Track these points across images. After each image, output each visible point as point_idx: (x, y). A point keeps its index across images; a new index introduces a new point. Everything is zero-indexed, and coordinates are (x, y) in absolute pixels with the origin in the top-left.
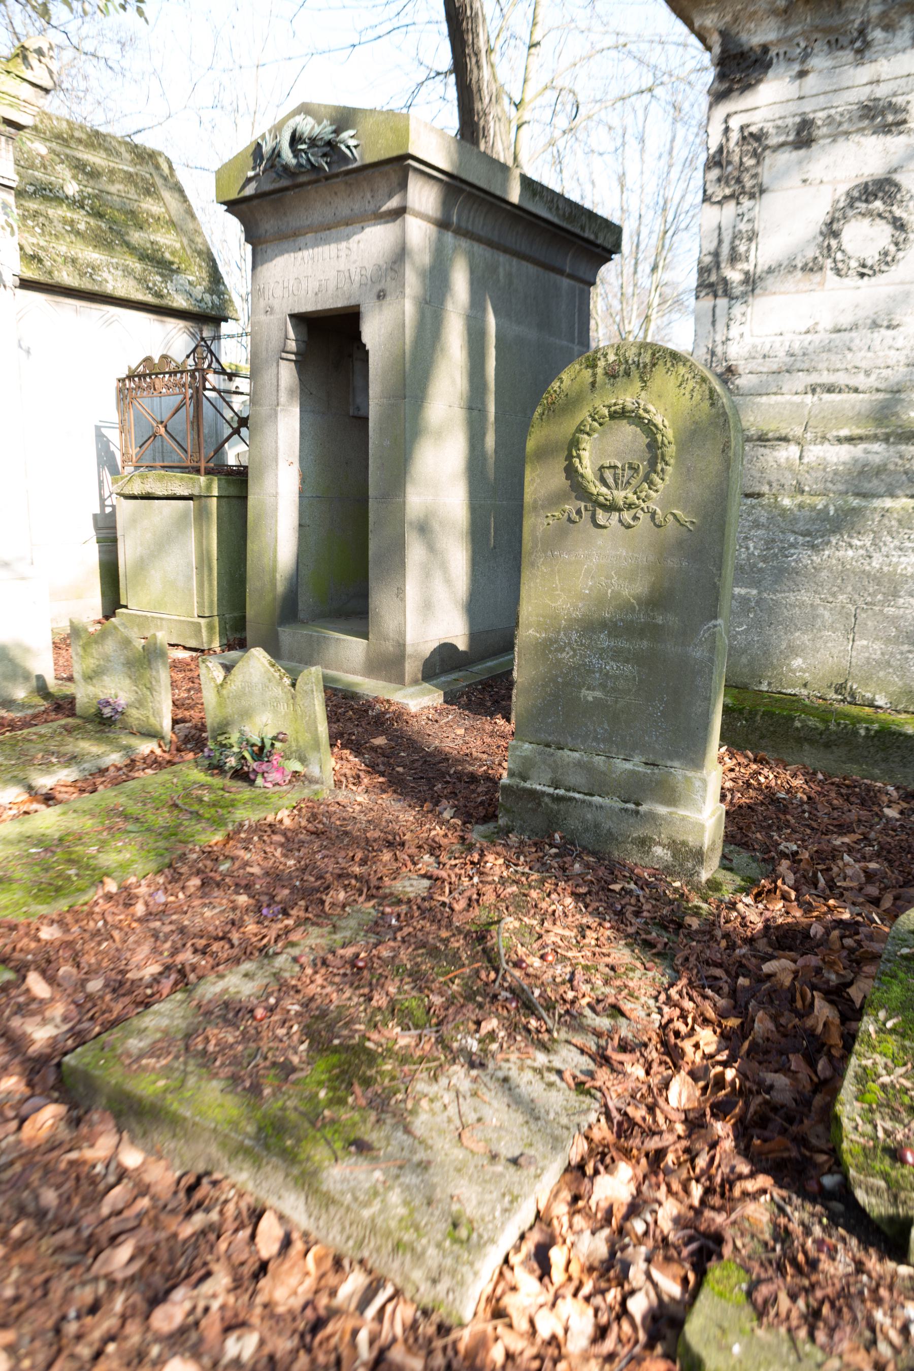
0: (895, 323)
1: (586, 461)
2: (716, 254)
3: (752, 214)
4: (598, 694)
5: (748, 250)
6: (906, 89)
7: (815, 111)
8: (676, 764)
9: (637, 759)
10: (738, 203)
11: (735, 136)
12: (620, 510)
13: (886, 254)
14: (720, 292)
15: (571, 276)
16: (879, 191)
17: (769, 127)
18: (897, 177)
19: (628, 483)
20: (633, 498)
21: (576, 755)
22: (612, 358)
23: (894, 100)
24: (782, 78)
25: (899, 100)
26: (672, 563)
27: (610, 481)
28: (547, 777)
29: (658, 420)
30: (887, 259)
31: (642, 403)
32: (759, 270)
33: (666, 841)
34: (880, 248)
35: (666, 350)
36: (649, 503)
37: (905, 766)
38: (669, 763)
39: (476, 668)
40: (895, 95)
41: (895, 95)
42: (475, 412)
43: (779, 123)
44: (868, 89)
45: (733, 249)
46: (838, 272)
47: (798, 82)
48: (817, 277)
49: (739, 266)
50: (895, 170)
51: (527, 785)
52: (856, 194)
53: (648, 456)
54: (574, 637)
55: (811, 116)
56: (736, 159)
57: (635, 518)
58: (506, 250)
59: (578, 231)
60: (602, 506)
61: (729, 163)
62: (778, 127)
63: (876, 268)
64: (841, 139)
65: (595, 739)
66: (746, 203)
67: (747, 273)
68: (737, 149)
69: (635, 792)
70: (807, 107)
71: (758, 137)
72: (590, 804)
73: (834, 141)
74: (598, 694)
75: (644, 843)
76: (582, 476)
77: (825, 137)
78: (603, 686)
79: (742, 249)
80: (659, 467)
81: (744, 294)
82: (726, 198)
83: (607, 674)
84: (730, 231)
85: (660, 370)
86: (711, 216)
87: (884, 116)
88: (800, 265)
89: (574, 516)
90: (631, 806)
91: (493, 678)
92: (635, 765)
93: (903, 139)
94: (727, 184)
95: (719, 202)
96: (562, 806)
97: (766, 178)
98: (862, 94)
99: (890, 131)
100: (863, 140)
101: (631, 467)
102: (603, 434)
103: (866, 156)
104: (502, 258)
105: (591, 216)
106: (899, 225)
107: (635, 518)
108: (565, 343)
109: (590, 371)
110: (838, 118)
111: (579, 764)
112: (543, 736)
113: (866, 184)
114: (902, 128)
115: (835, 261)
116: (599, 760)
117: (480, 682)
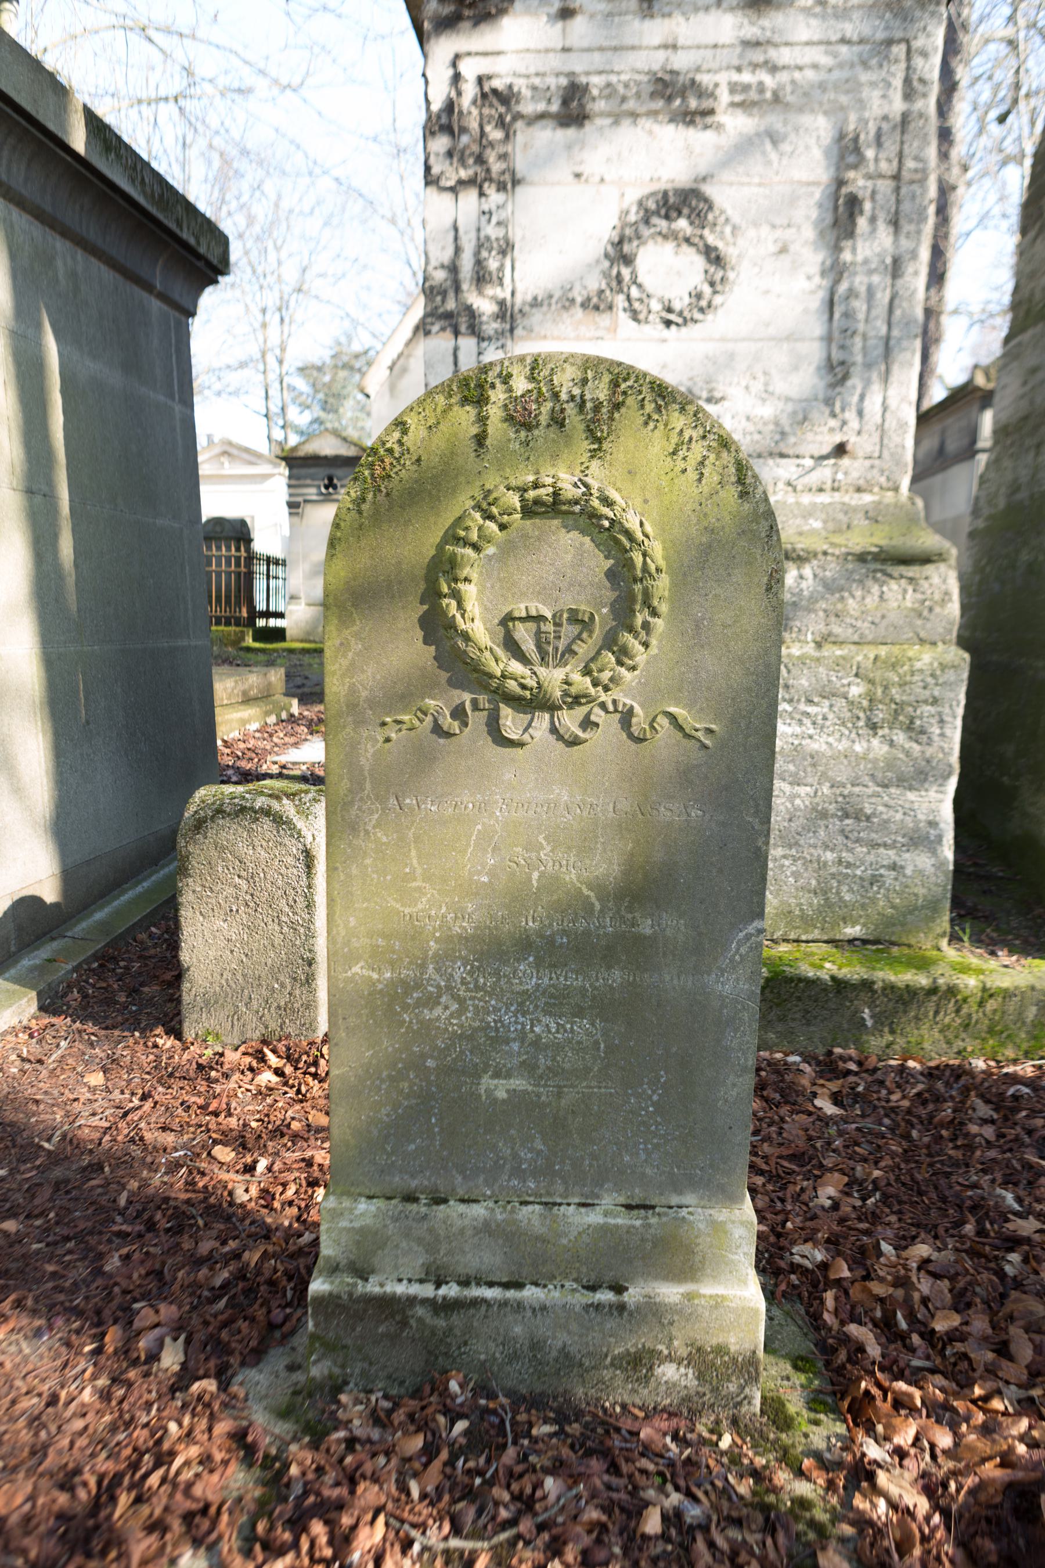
0: (717, 395)
1: (472, 606)
2: (453, 269)
3: (503, 215)
4: (518, 1083)
5: (501, 268)
6: (714, 65)
7: (588, 74)
8: (689, 1199)
9: (608, 1200)
10: (482, 194)
11: (470, 90)
12: (552, 708)
13: (699, 296)
14: (463, 328)
15: (163, 297)
16: (681, 206)
17: (521, 85)
18: (708, 190)
19: (570, 651)
20: (582, 683)
21: (478, 1211)
22: (521, 385)
23: (698, 78)
24: (536, 14)
25: (705, 79)
26: (670, 813)
27: (529, 646)
28: (416, 1262)
29: (632, 522)
30: (701, 305)
31: (595, 484)
32: (519, 300)
33: (683, 1352)
34: (691, 288)
35: (641, 376)
36: (616, 693)
37: (808, 1024)
38: (675, 1200)
39: (81, 927)
40: (698, 69)
41: (698, 69)
42: (38, 499)
43: (537, 81)
44: (661, 55)
45: (479, 263)
46: (635, 316)
47: (560, 25)
48: (604, 320)
49: (490, 291)
50: (704, 179)
51: (372, 1287)
52: (652, 205)
53: (610, 595)
54: (459, 972)
55: (583, 80)
56: (474, 125)
57: (587, 723)
58: (65, 233)
59: (173, 226)
60: (513, 700)
61: (463, 130)
62: (534, 88)
63: (686, 314)
64: (626, 122)
65: (517, 1172)
66: (495, 197)
67: (502, 303)
68: (475, 112)
69: (606, 1269)
70: (578, 64)
71: (505, 98)
72: (519, 1306)
73: (616, 123)
74: (518, 1083)
75: (639, 1364)
76: (466, 637)
77: (602, 114)
78: (529, 1068)
79: (493, 264)
80: (639, 619)
81: (500, 334)
82: (461, 182)
83: (536, 1043)
84: (473, 235)
85: (630, 416)
86: (442, 208)
87: (684, 98)
88: (579, 300)
89: (448, 722)
90: (605, 1296)
91: (113, 944)
92: (604, 1214)
93: (709, 135)
94: (462, 162)
95: (452, 189)
96: (457, 1320)
97: (520, 165)
98: (656, 61)
99: (692, 122)
100: (656, 128)
101: (574, 617)
102: (508, 550)
103: (656, 154)
104: (60, 245)
105: (190, 209)
106: (714, 257)
107: (587, 723)
108: (162, 398)
109: (471, 411)
110: (621, 90)
111: (486, 1229)
112: (398, 1181)
113: (665, 193)
114: (709, 120)
115: (629, 298)
116: (530, 1215)
117: (95, 957)
